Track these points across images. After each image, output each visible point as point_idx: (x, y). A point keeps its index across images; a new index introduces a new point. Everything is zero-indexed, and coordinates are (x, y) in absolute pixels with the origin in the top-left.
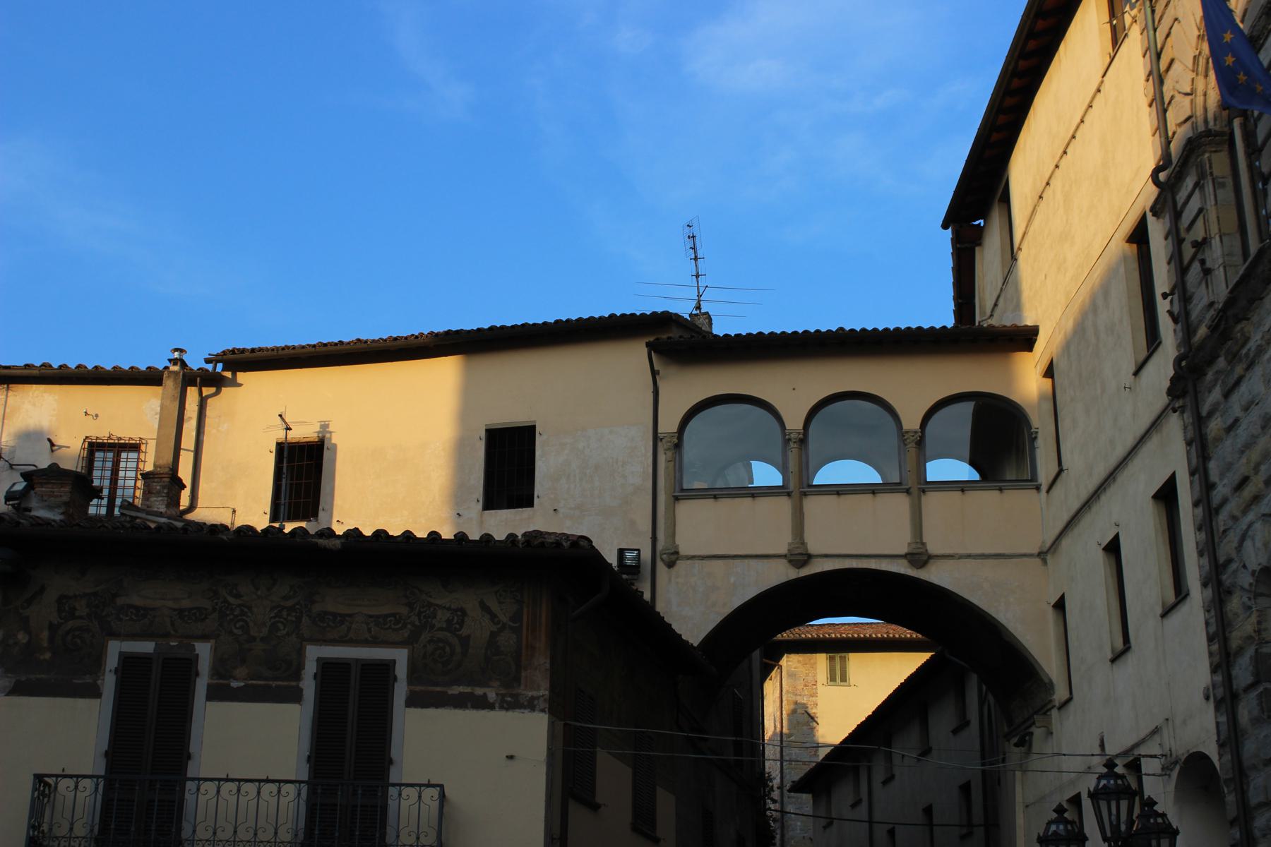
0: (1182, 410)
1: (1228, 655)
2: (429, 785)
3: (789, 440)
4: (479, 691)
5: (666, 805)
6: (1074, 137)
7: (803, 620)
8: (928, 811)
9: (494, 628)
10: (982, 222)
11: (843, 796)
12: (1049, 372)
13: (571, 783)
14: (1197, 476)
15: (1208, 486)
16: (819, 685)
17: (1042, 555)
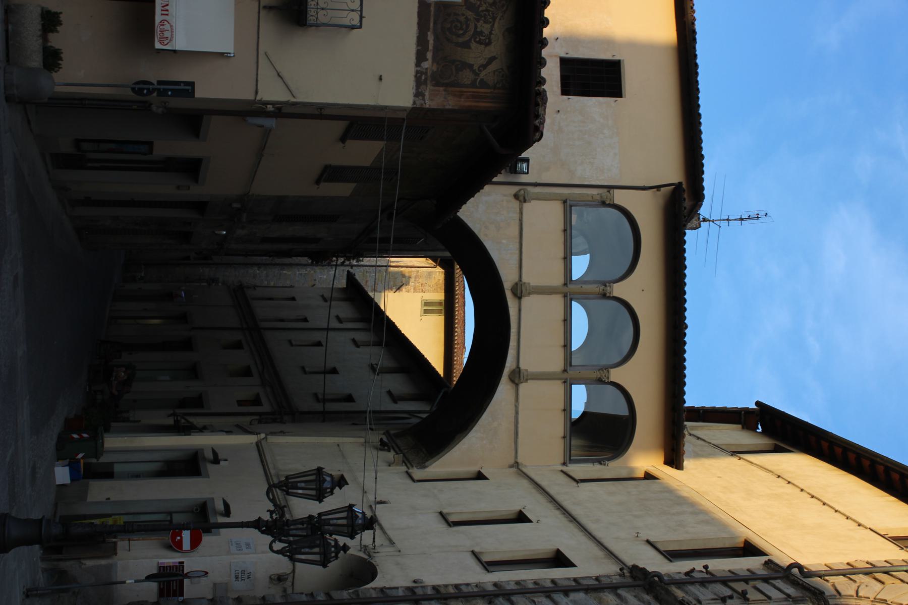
0: (622, 575)
1: (446, 599)
2: (361, 17)
3: (606, 286)
4: (429, 55)
5: (343, 189)
6: (824, 504)
7: (465, 272)
8: (334, 371)
9: (476, 67)
10: (760, 430)
11: (344, 310)
12: (648, 476)
13: (360, 123)
14: (574, 584)
15: (566, 592)
16: (422, 294)
17: (516, 465)
